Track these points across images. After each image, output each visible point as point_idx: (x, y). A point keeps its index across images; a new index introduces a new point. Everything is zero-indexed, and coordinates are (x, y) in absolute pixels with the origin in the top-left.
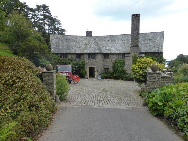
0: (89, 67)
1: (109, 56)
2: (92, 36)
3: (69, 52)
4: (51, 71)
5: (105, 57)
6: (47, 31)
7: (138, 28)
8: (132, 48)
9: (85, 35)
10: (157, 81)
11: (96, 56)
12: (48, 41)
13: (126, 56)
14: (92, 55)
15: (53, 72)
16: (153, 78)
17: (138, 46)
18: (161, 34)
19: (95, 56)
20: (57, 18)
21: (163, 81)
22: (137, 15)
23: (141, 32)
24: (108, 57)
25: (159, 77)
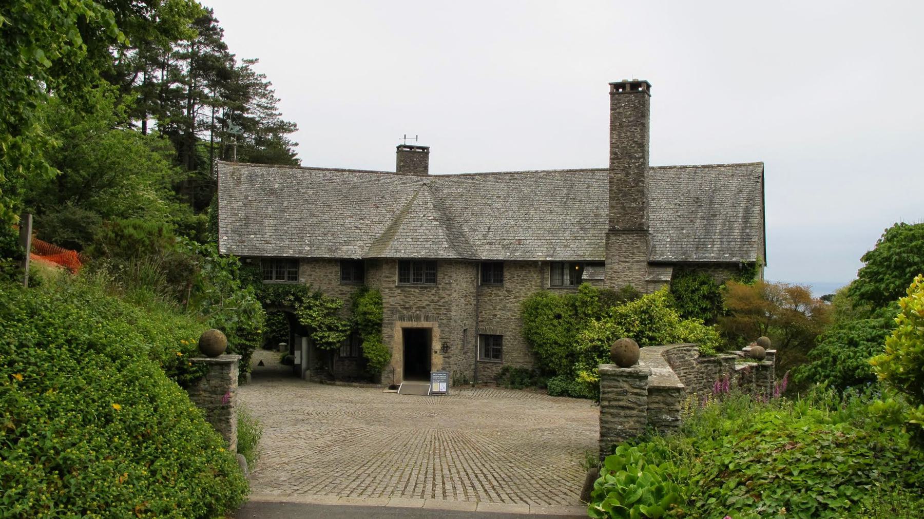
0: (407, 332)
1: (507, 275)
2: (432, 171)
3: (306, 250)
4: (223, 358)
5: (485, 281)
6: (205, 136)
7: (642, 146)
8: (613, 239)
9: (390, 164)
10: (631, 405)
11: (440, 276)
12: (201, 194)
13: (584, 277)
14: (420, 271)
15: (228, 364)
16: (618, 394)
17: (641, 231)
18: (753, 178)
19: (435, 275)
20: (252, 67)
21: (656, 406)
22: (635, 85)
23: (656, 159)
24: (500, 281)
25: (638, 391)
